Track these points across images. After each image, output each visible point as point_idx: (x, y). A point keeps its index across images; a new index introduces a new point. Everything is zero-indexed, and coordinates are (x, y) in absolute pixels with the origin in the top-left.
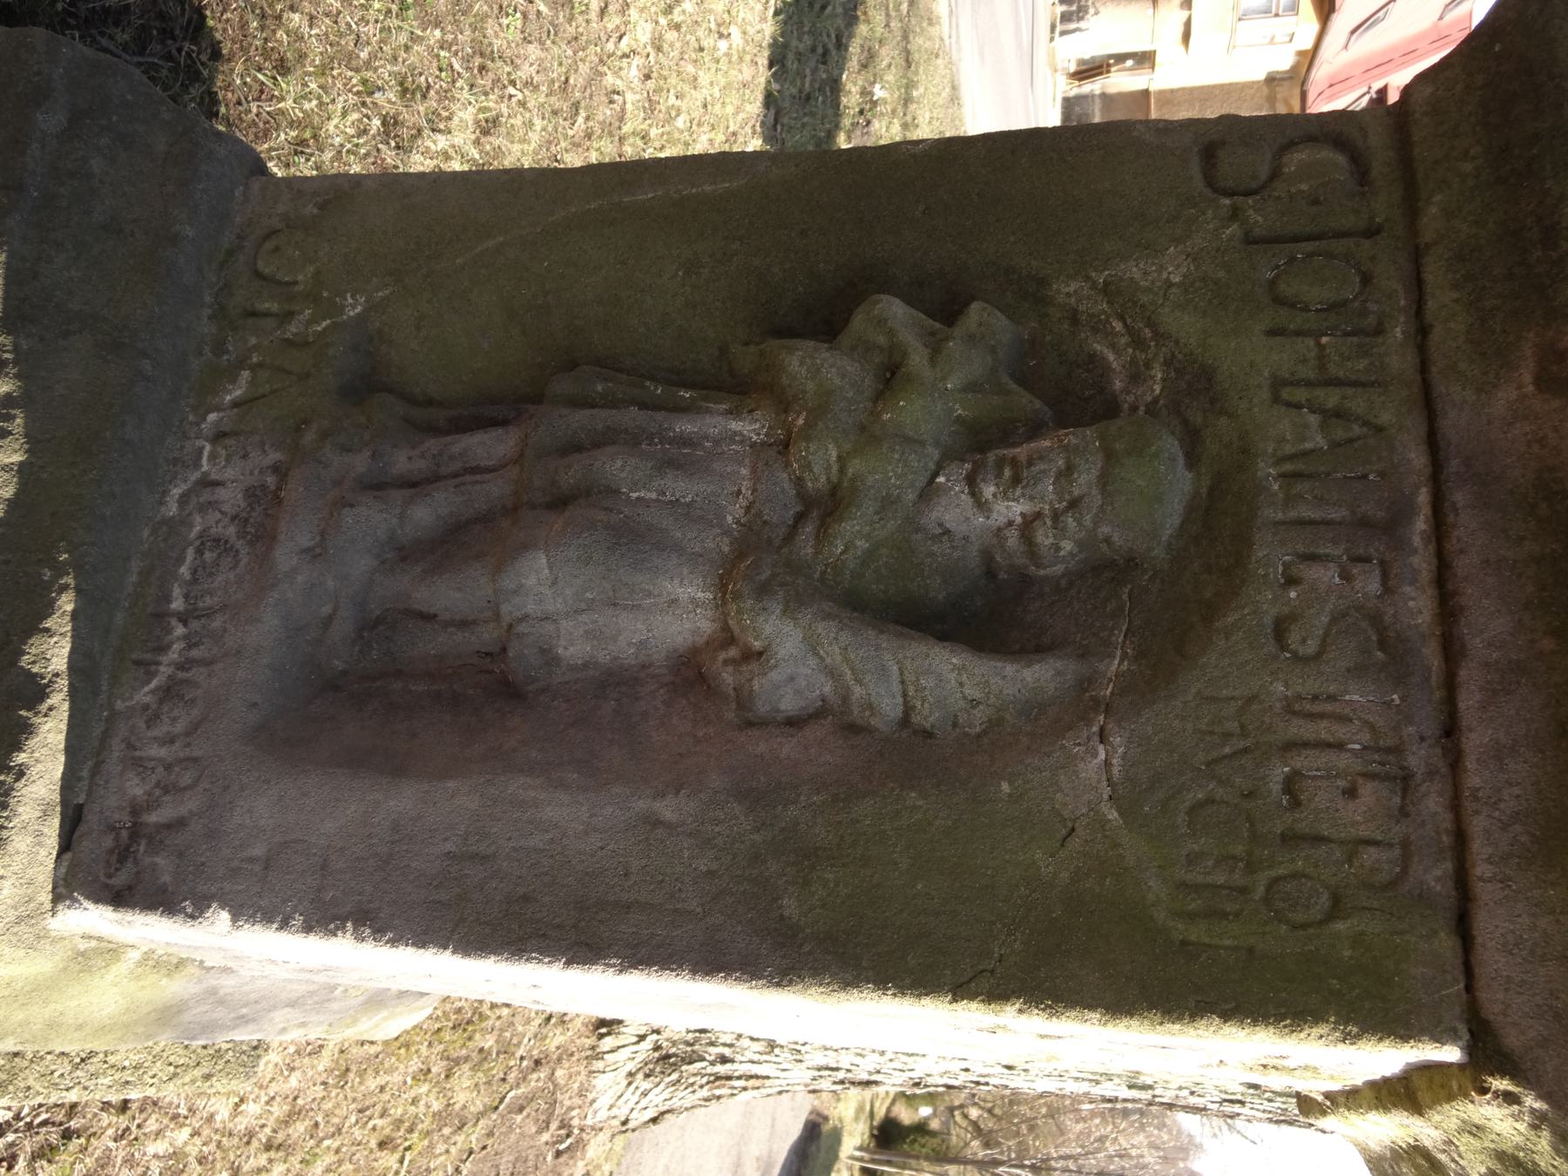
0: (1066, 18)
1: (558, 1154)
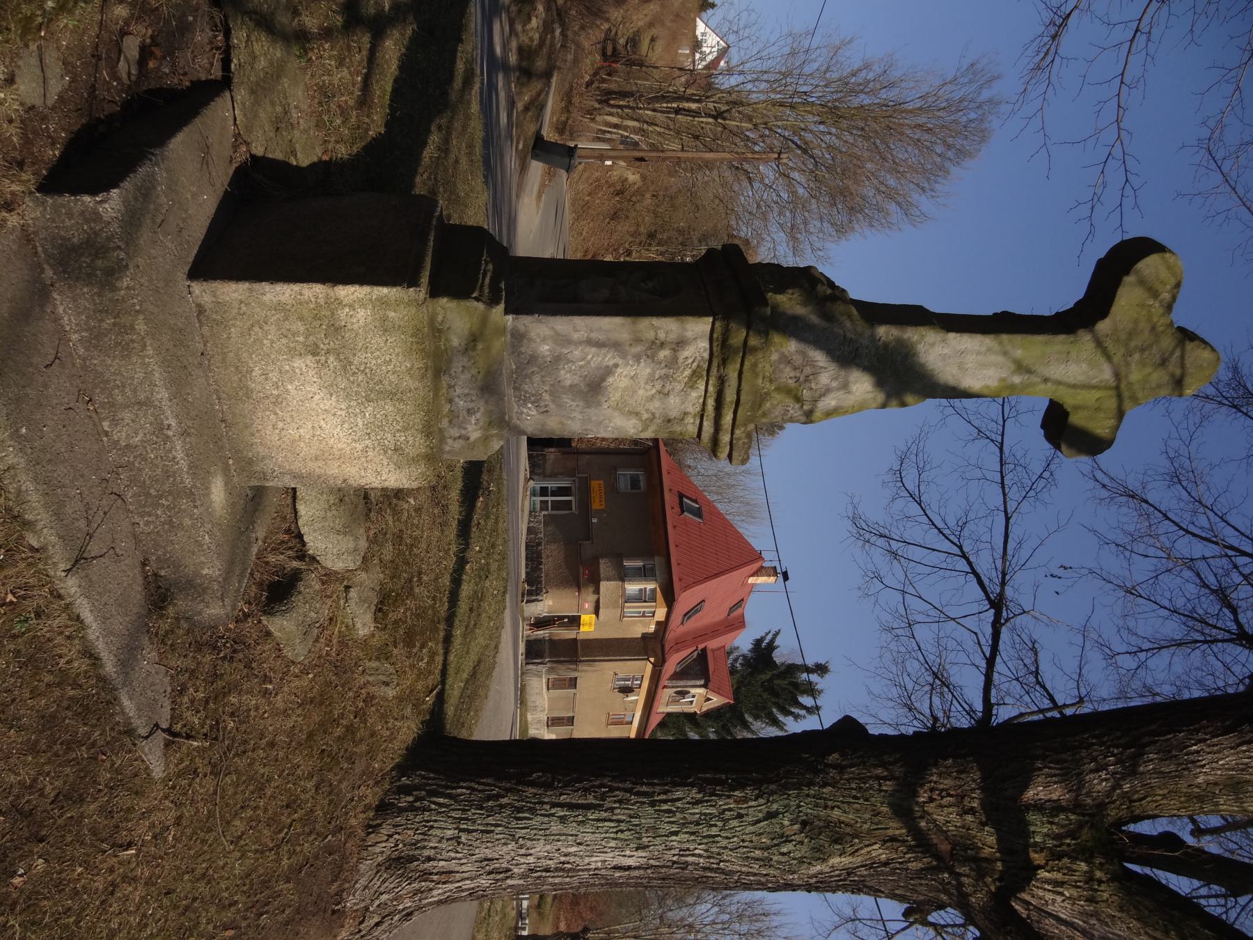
0: (530, 593)
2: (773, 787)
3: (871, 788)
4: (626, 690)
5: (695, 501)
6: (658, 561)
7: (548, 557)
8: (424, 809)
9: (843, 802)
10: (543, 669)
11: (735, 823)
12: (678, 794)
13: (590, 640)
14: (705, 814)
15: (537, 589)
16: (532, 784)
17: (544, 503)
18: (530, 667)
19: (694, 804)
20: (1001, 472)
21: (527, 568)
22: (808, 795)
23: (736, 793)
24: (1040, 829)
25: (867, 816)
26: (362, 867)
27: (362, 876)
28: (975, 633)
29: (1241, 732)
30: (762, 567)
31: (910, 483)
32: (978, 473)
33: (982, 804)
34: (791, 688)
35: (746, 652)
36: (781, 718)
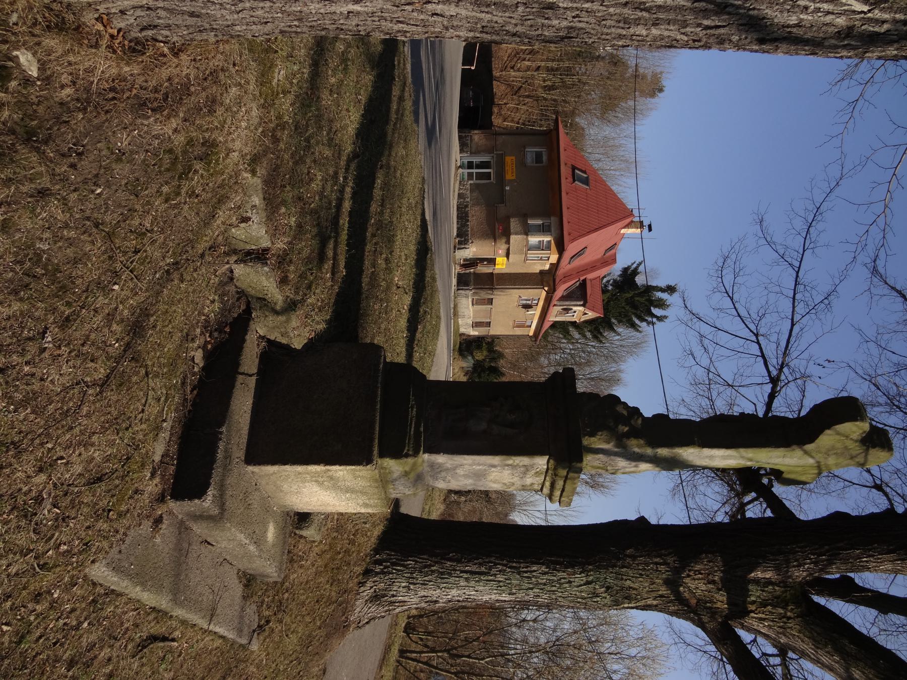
1: (344, 627)
2: (590, 567)
3: (652, 569)
4: (527, 307)
5: (584, 172)
6: (554, 220)
7: (473, 216)
8: (390, 573)
9: (633, 577)
10: (470, 293)
11: (567, 585)
12: (534, 568)
13: (502, 274)
14: (549, 580)
15: (465, 240)
16: (450, 560)
17: (470, 176)
18: (460, 292)
19: (543, 574)
20: (795, 290)
21: (458, 224)
22: (612, 572)
23: (569, 570)
24: (755, 594)
25: (646, 584)
26: (357, 603)
27: (358, 607)
28: (755, 404)
29: (899, 554)
30: (632, 222)
31: (728, 279)
32: (777, 289)
33: (721, 579)
34: (647, 303)
35: (615, 277)
36: (637, 322)
